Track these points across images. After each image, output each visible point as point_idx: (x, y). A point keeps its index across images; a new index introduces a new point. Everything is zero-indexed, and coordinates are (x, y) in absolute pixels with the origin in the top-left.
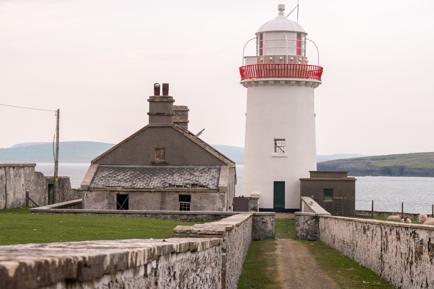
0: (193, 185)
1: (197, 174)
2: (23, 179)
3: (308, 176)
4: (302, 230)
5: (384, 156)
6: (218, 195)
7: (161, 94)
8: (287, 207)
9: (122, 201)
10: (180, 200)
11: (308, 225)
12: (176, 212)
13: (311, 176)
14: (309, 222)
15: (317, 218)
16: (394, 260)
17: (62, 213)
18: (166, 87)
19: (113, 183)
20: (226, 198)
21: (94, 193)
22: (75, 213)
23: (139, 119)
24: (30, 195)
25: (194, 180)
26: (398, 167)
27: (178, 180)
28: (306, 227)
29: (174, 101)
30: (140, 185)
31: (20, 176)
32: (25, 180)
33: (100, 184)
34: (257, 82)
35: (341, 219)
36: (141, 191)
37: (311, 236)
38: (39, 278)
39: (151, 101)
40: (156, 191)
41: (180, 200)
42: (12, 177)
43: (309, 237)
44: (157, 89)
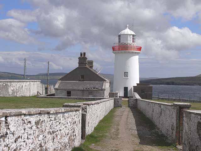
2: (36, 86)
3: (136, 85)
4: (131, 104)
5: (150, 79)
6: (102, 91)
7: (83, 56)
8: (128, 96)
9: (69, 93)
11: (134, 102)
12: (155, 101)
13: (137, 85)
14: (134, 101)
15: (136, 100)
16: (155, 115)
18: (85, 54)
20: (105, 93)
21: (59, 91)
22: (53, 98)
23: (74, 64)
26: (172, 82)
28: (133, 103)
29: (87, 59)
30: (75, 88)
31: (35, 85)
32: (37, 86)
34: (118, 52)
35: (73, 98)
36: (74, 90)
37: (135, 106)
39: (79, 58)
42: (32, 85)
44: (81, 54)
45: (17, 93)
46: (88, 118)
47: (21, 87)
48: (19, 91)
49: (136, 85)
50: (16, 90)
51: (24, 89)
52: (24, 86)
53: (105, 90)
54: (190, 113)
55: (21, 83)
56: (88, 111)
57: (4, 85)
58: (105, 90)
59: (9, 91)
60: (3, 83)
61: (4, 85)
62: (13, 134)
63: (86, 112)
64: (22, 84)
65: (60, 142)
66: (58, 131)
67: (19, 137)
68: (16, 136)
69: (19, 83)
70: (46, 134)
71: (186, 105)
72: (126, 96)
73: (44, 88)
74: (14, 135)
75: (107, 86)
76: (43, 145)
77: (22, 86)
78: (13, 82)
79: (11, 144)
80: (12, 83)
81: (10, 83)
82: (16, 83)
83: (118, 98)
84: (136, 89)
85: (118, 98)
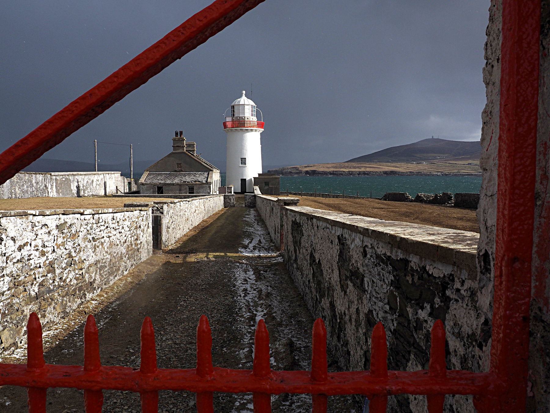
0: (195, 181)
1: (197, 176)
3: (257, 176)
10: (457, 195)
15: (255, 196)
17: (129, 196)
18: (181, 133)
19: (155, 181)
24: (118, 188)
25: (195, 179)
27: (188, 179)
28: (250, 200)
30: (168, 182)
33: (148, 182)
38: (322, 349)
40: (178, 184)
41: (457, 195)
43: (251, 205)
44: (177, 134)
45: (84, 191)
46: (165, 221)
47: (90, 182)
48: (87, 188)
49: (257, 176)
50: (83, 186)
51: (94, 184)
52: (95, 180)
53: (210, 183)
54: (288, 209)
55: (90, 177)
56: (165, 213)
57: (64, 179)
58: (210, 183)
59: (72, 188)
60: (61, 177)
61: (64, 179)
62: (13, 239)
63: (162, 213)
64: (92, 177)
65: (109, 252)
66: (103, 237)
67: (26, 244)
68: (18, 244)
69: (87, 177)
70: (80, 241)
71: (292, 200)
72: (243, 191)
73: (126, 183)
74: (17, 241)
75: (216, 176)
76: (74, 254)
77: (93, 181)
78: (78, 174)
79: (11, 253)
80: (76, 177)
81: (73, 177)
82: (83, 177)
83: (233, 193)
84: (257, 181)
85: (233, 193)
